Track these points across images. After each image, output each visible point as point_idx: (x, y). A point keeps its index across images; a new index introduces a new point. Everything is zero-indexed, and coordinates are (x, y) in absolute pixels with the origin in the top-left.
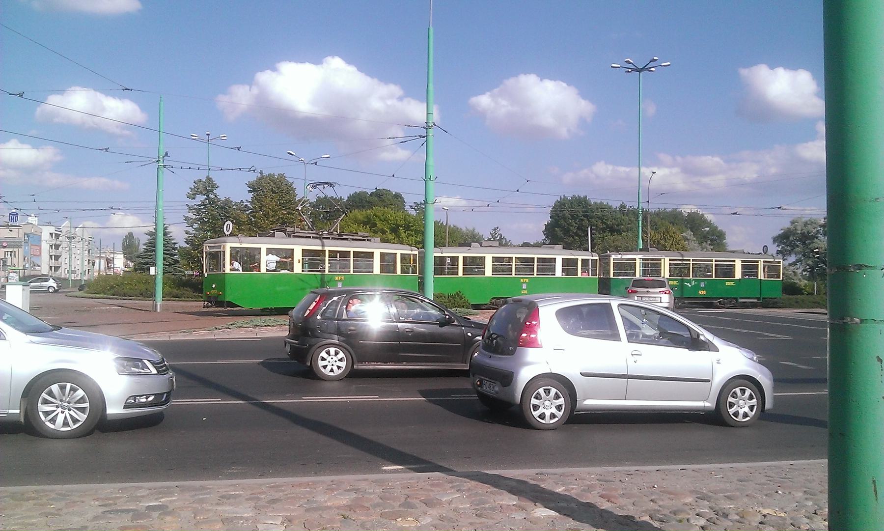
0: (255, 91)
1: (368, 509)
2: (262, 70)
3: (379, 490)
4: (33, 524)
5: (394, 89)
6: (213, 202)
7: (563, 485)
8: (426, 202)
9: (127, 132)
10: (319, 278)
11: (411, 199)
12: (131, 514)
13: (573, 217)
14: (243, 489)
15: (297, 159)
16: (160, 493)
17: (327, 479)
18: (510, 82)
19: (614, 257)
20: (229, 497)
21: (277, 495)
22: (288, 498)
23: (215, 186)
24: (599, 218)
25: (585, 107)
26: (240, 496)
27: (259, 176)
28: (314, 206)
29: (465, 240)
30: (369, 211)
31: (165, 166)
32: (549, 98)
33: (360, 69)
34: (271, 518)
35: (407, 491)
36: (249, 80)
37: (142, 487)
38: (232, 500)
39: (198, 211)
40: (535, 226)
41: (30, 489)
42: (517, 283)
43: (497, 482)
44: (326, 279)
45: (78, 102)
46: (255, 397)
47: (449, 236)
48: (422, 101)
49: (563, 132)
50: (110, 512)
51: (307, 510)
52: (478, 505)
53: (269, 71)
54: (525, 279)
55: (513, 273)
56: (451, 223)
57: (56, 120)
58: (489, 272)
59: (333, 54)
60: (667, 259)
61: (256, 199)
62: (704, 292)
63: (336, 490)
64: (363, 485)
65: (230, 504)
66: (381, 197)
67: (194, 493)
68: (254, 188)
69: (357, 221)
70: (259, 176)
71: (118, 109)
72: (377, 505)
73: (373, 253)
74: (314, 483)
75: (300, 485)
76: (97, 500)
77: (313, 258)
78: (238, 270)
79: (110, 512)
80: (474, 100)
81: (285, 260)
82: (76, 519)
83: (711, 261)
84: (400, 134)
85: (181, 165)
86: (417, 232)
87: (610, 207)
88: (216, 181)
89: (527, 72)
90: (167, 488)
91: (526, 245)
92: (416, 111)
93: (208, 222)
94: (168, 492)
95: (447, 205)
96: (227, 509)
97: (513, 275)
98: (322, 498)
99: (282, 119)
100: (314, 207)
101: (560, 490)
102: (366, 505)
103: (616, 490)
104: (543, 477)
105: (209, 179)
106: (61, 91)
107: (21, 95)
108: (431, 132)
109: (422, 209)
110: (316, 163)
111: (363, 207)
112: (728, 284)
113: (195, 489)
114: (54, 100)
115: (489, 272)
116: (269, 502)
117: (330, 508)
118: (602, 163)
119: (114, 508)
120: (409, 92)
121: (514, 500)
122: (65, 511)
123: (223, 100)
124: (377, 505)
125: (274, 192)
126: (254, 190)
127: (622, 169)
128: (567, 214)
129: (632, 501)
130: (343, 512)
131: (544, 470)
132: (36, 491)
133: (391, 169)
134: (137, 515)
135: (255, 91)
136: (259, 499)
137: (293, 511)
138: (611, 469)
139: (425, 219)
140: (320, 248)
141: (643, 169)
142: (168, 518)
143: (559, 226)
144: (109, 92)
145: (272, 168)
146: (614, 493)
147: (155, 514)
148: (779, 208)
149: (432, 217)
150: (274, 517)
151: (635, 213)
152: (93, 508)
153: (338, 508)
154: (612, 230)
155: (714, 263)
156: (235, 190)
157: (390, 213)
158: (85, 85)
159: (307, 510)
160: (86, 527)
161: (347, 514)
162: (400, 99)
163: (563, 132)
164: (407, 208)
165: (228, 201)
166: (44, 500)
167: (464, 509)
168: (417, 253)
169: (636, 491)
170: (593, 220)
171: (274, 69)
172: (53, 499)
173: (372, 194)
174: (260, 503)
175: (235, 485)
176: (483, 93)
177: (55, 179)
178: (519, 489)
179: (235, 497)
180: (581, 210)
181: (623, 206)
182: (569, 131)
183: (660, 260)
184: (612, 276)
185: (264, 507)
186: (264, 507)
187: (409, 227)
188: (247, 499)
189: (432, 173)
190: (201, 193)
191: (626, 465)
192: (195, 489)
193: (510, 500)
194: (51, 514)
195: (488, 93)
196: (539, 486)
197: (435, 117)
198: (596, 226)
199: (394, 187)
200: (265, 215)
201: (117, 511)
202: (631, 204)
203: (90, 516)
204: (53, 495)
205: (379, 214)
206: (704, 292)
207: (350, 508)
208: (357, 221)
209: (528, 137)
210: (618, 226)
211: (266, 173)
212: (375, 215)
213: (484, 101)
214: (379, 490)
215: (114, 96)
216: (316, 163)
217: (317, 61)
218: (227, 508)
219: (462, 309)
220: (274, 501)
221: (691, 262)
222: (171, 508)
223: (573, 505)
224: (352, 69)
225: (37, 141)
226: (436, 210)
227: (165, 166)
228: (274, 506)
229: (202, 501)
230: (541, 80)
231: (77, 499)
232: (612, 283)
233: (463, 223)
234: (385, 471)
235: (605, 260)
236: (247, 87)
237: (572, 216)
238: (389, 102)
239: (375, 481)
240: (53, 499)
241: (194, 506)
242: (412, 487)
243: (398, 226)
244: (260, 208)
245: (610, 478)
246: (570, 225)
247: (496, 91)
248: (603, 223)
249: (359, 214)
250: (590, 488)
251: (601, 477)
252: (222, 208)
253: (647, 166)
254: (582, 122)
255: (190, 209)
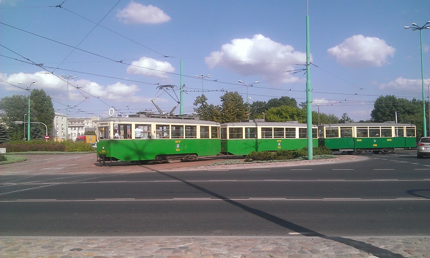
0: (222, 54)
1: (282, 253)
2: (225, 44)
3: (287, 244)
4: (130, 254)
5: (289, 48)
6: (205, 106)
7: (384, 245)
8: (307, 102)
9: (166, 76)
10: (255, 141)
11: (299, 102)
12: (172, 250)
13: (387, 107)
14: (222, 240)
15: (243, 84)
16: (185, 241)
17: (262, 237)
18: (349, 40)
19: (229, 126)
20: (216, 244)
21: (238, 244)
22: (244, 246)
23: (206, 99)
24: (402, 107)
25: (390, 50)
26: (221, 243)
27: (226, 93)
28: (252, 106)
29: (333, 120)
30: (279, 108)
31: (183, 91)
32: (370, 46)
33: (272, 39)
34: (235, 255)
35: (301, 245)
36: (219, 49)
37: (177, 238)
38: (217, 245)
39: (199, 111)
40: (366, 113)
41: (129, 238)
42: (371, 141)
43: (349, 242)
44: (259, 142)
45: (144, 64)
46: (227, 197)
47: (319, 119)
48: (303, 52)
49: (379, 63)
50: (163, 249)
51: (253, 252)
52: (338, 253)
53: (228, 44)
54: (279, 140)
55: (285, 136)
56: (321, 112)
57: (136, 72)
58: (297, 136)
59: (258, 33)
60: (355, 127)
61: (224, 104)
62: (376, 145)
63: (267, 243)
64: (280, 241)
65: (216, 248)
66: (285, 101)
67: (200, 242)
68: (223, 99)
69: (273, 113)
70: (226, 93)
71: (162, 66)
72: (286, 251)
73: (196, 126)
74: (256, 239)
75: (249, 240)
76: (158, 243)
77: (267, 132)
78: (118, 138)
79: (163, 249)
80: (330, 50)
81: (400, 132)
82: (149, 252)
83: (379, 127)
84: (293, 69)
85: (190, 90)
86: (303, 117)
87: (407, 101)
88: (206, 96)
89: (357, 34)
90: (189, 239)
91: (361, 122)
92: (301, 58)
93: (203, 116)
94: (189, 241)
95: (318, 103)
96: (215, 250)
97: (273, 138)
98: (260, 247)
99: (234, 66)
100: (252, 107)
101: (382, 247)
102: (281, 251)
103: (413, 248)
104: (373, 240)
105: (203, 96)
106: (137, 59)
107: (121, 62)
108: (309, 67)
109: (305, 105)
110: (252, 86)
111: (276, 106)
112: (388, 140)
113: (200, 240)
114: (135, 63)
115: (297, 136)
116: (234, 247)
117: (264, 251)
118: (401, 78)
119: (165, 247)
120: (297, 49)
121: (357, 251)
122: (144, 248)
123: (208, 59)
124: (286, 251)
125: (233, 101)
126: (224, 100)
127: (412, 81)
128: (383, 105)
129: (422, 254)
130: (271, 254)
131: (373, 237)
132: (132, 239)
133: (287, 85)
134: (175, 251)
135: (222, 54)
136: (230, 245)
137: (246, 252)
138: (410, 237)
139: (307, 110)
140: (255, 127)
141: (424, 80)
142: (189, 253)
143: (379, 111)
144: (158, 59)
145: (232, 89)
146: (412, 249)
147: (183, 251)
148: (28, 59)
149: (310, 110)
150: (237, 255)
151: (421, 103)
152: (155, 247)
153: (268, 251)
154: (409, 113)
155: (368, 129)
156: (215, 101)
157: (290, 109)
158: (148, 56)
159: (253, 252)
160: (153, 256)
161: (272, 255)
162: (292, 52)
163: (379, 63)
164: (298, 105)
165: (212, 106)
166: (135, 243)
167: (331, 255)
168: (220, 126)
169: (424, 248)
170: (398, 108)
171: (231, 43)
172: (139, 243)
173: (280, 99)
174: (231, 248)
175: (218, 239)
176: (334, 46)
177: (136, 99)
178: (360, 246)
179: (219, 244)
180: (391, 102)
181: (414, 100)
182: (381, 62)
183: (403, 127)
184: (325, 137)
185: (232, 249)
186: (232, 249)
187: (299, 115)
188: (224, 246)
189: (310, 87)
190: (200, 102)
191: (419, 235)
192: (200, 240)
193: (355, 251)
194: (138, 249)
195: (337, 47)
196: (371, 245)
197: (311, 60)
198: (400, 111)
199: (291, 95)
200: (229, 111)
201: (166, 249)
202: (419, 98)
203: (154, 251)
204: (139, 241)
205: (284, 109)
206: (376, 145)
207: (273, 252)
208: (273, 113)
209: (360, 67)
210: (412, 110)
211: (229, 92)
212: (282, 109)
213: (335, 50)
214: (287, 244)
215: (160, 60)
216: (252, 86)
217: (250, 36)
218: (215, 249)
219: (328, 155)
220: (237, 247)
221: (380, 129)
222: (190, 248)
223: (389, 255)
224: (268, 39)
225: (128, 82)
226: (313, 106)
227: (183, 91)
228: (237, 249)
229: (204, 245)
230: (365, 37)
231: (149, 243)
232: (229, 144)
233: (327, 112)
234: (291, 235)
235: (321, 128)
236: (219, 52)
237: (386, 106)
238: (287, 54)
239: (286, 240)
240: (139, 243)
241: (201, 247)
242: (304, 243)
243: (294, 114)
244: (227, 108)
245: (410, 242)
246: (385, 110)
247: (341, 45)
248: (404, 109)
249: (274, 109)
250: (398, 247)
251: (405, 241)
252: (209, 109)
253: (426, 79)
254: (389, 57)
255: (195, 110)
